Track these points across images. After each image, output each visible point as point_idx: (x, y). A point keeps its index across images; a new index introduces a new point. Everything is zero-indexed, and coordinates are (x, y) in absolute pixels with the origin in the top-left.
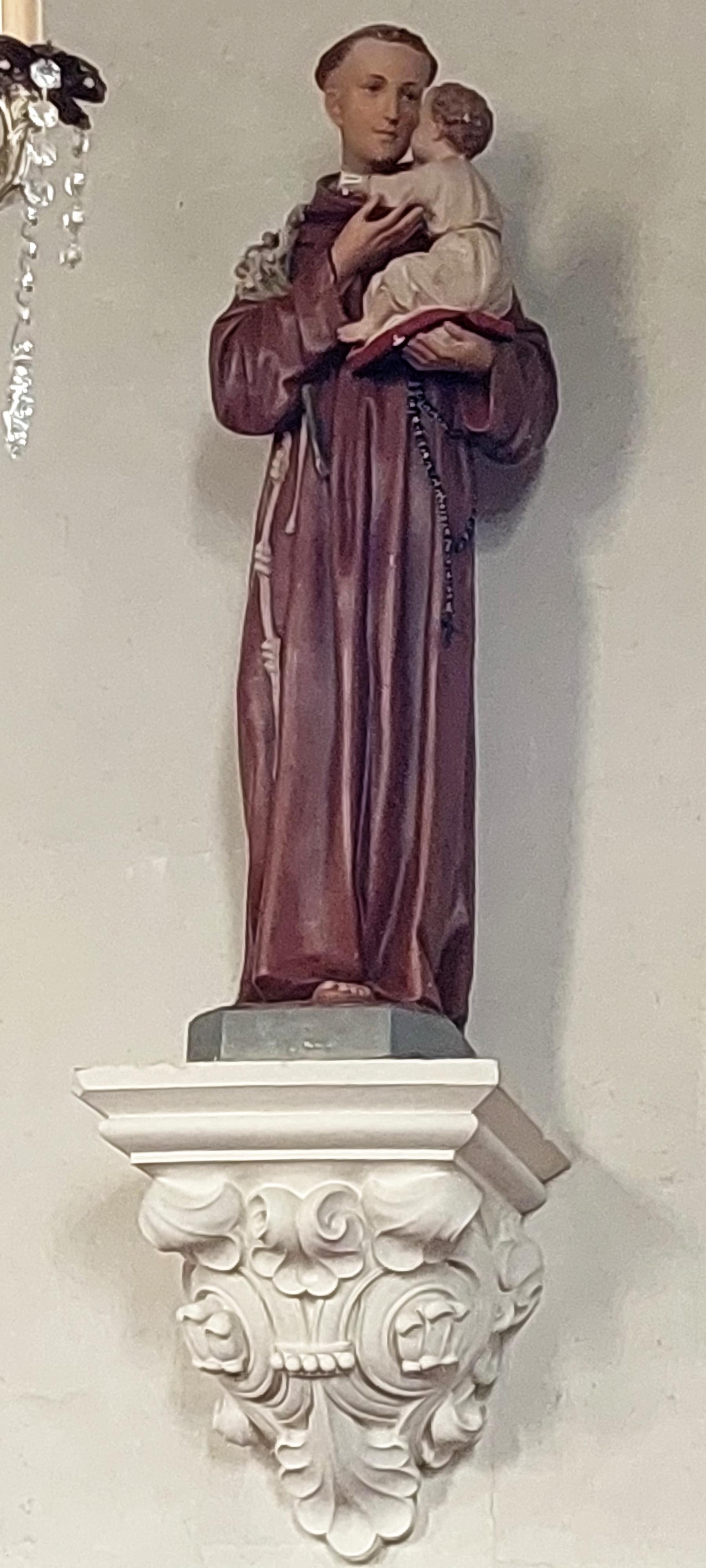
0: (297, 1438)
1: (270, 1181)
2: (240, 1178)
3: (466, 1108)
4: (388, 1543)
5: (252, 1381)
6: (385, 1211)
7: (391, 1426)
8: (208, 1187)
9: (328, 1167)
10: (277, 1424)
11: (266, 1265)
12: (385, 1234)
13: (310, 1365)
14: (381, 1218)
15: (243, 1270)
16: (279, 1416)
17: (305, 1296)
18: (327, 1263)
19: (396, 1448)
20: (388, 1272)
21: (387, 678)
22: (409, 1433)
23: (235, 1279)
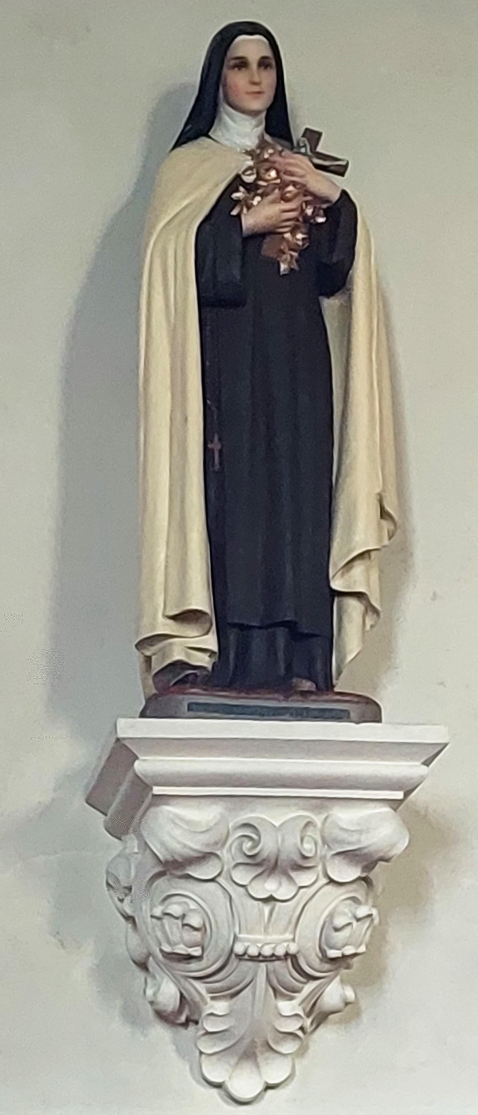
0: (221, 1007)
1: (252, 811)
2: (230, 810)
3: (417, 760)
4: (269, 1087)
5: (204, 963)
6: (345, 836)
7: (292, 998)
8: (205, 815)
9: (301, 802)
10: (207, 996)
11: (242, 876)
12: (339, 854)
13: (267, 951)
14: (338, 841)
15: (219, 879)
16: (210, 991)
17: (270, 899)
18: (293, 874)
19: (297, 1015)
20: (331, 881)
21: (160, 578)
22: (304, 1005)
23: (211, 885)
